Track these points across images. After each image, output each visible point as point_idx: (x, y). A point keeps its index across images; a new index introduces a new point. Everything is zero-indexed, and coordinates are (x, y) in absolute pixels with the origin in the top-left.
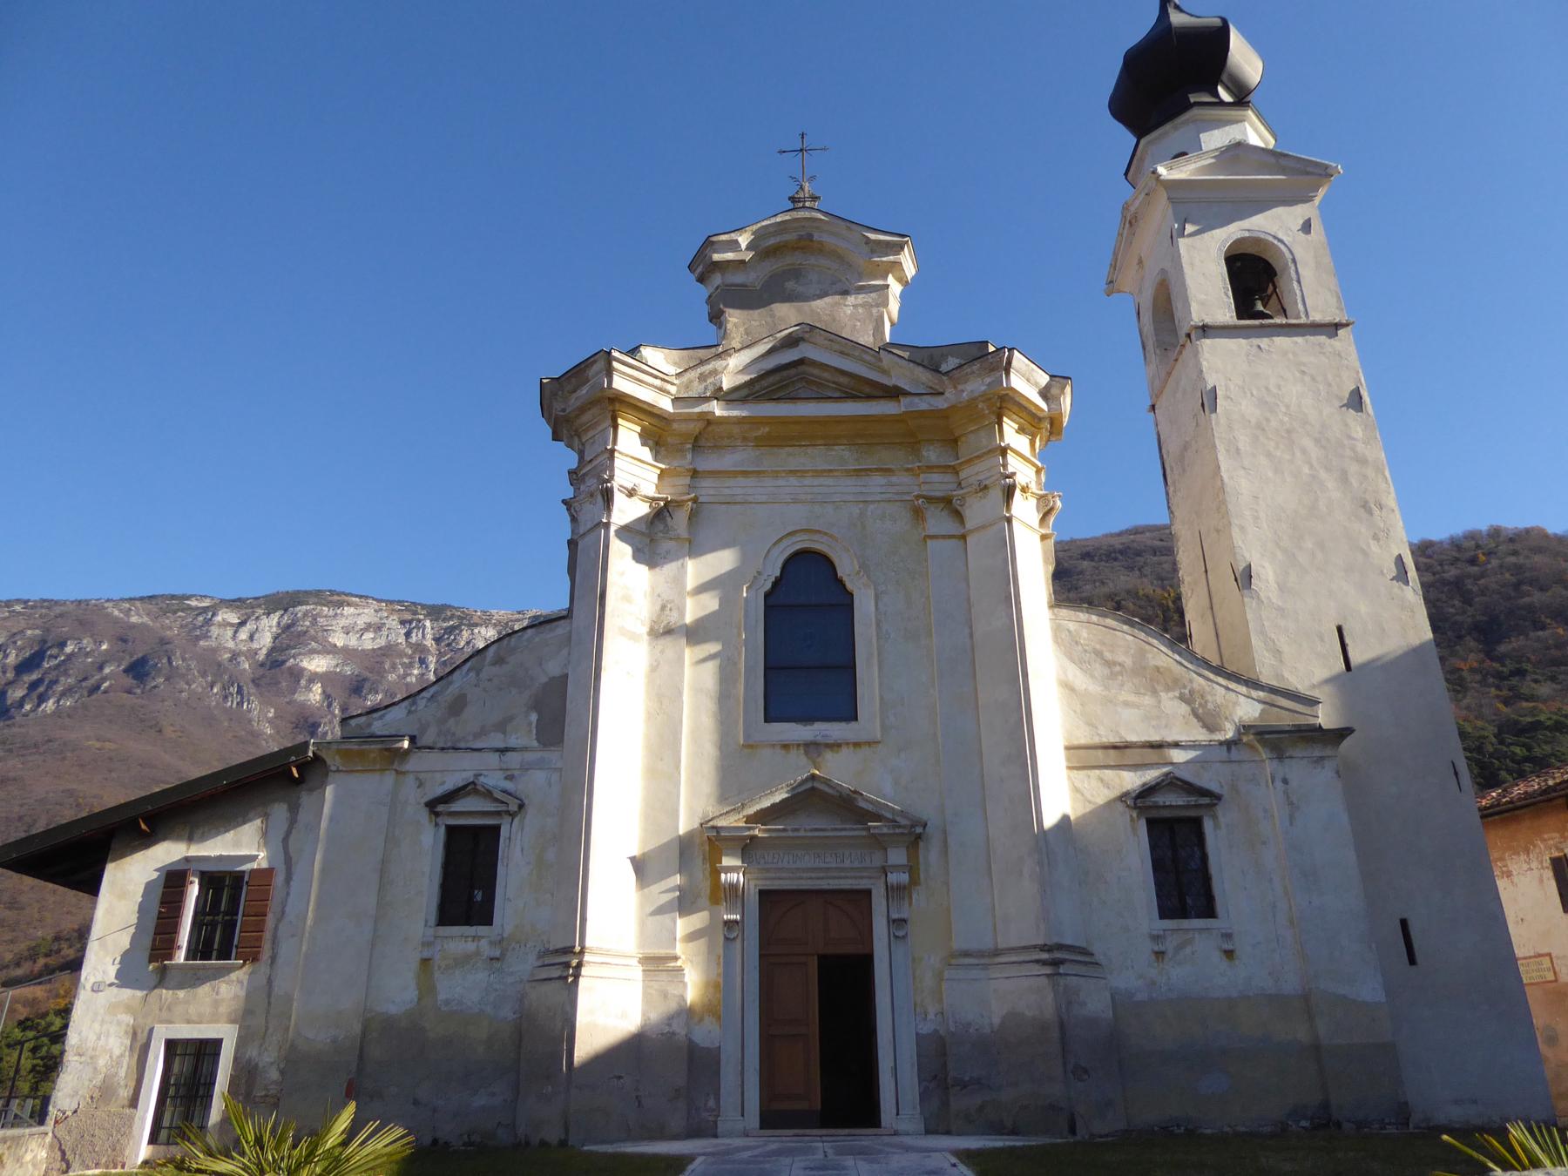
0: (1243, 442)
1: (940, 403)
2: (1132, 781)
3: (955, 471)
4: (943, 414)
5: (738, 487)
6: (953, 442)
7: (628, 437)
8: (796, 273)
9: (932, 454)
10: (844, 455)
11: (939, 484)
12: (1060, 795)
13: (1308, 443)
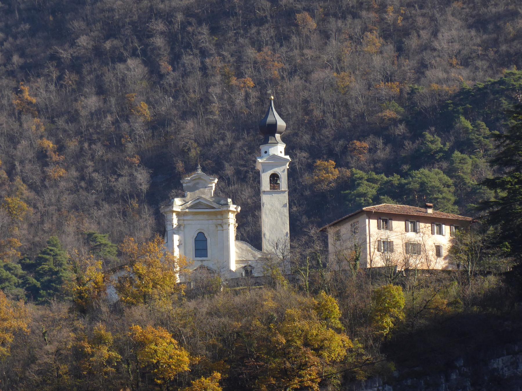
0: (267, 212)
1: (220, 210)
2: (243, 265)
3: (222, 220)
4: (221, 211)
5: (190, 222)
6: (222, 215)
7: (174, 214)
8: (198, 183)
9: (219, 217)
10: (206, 216)
11: (220, 222)
12: (233, 267)
13: (277, 213)
